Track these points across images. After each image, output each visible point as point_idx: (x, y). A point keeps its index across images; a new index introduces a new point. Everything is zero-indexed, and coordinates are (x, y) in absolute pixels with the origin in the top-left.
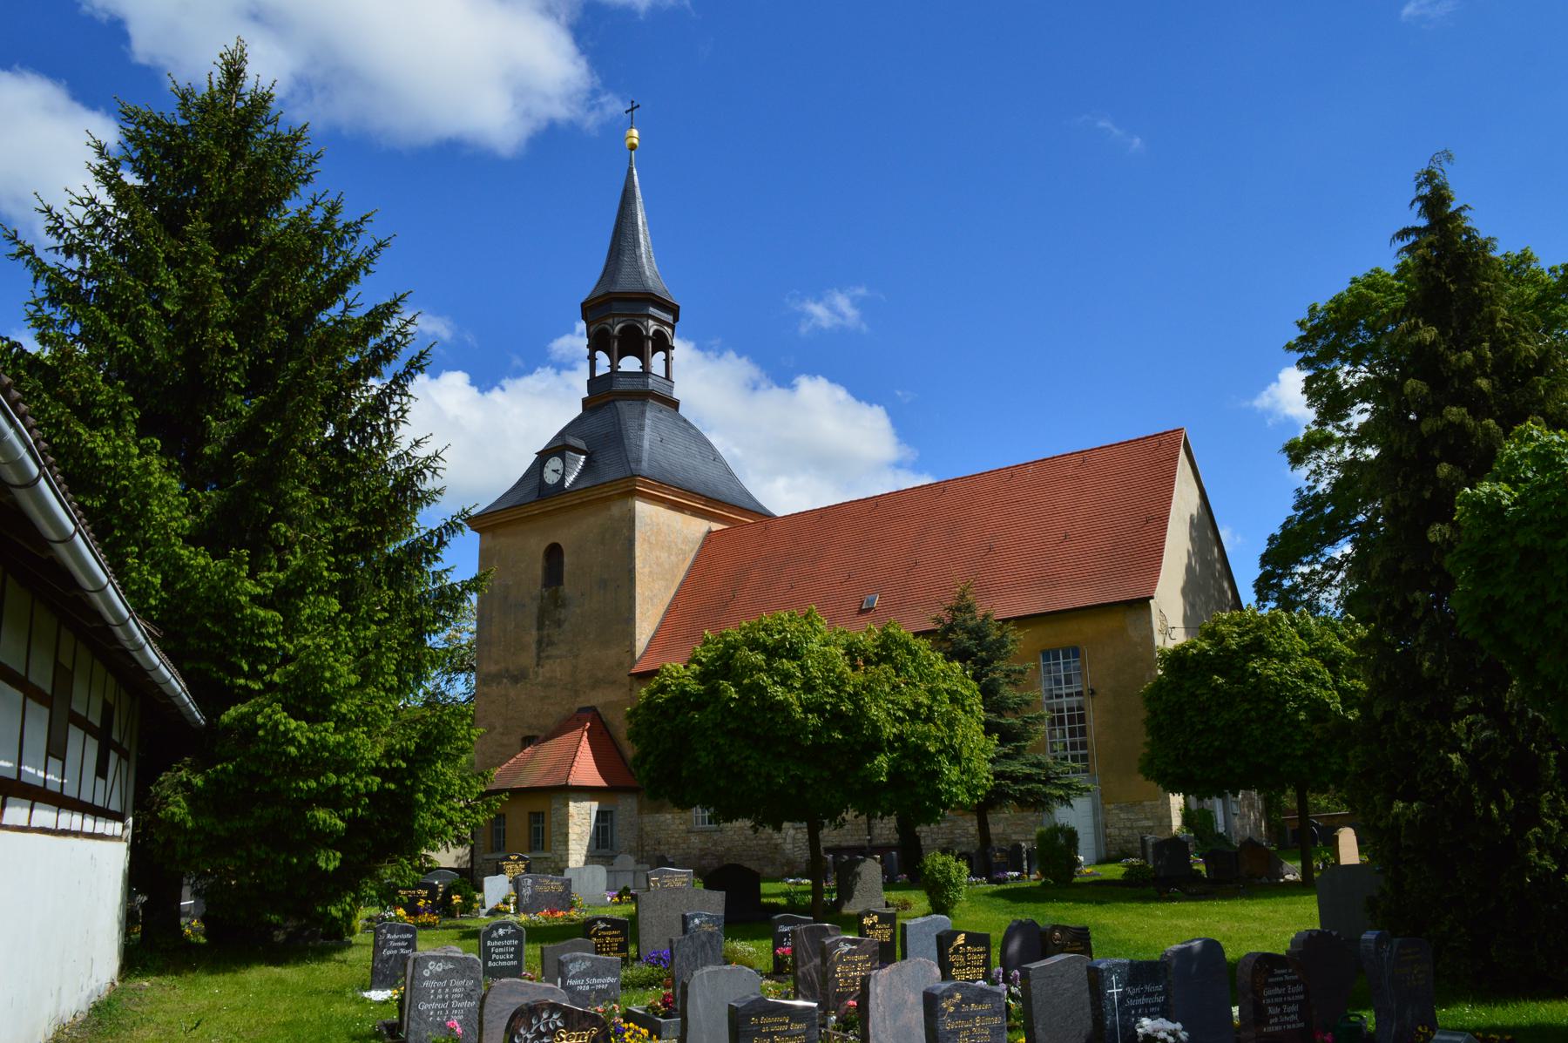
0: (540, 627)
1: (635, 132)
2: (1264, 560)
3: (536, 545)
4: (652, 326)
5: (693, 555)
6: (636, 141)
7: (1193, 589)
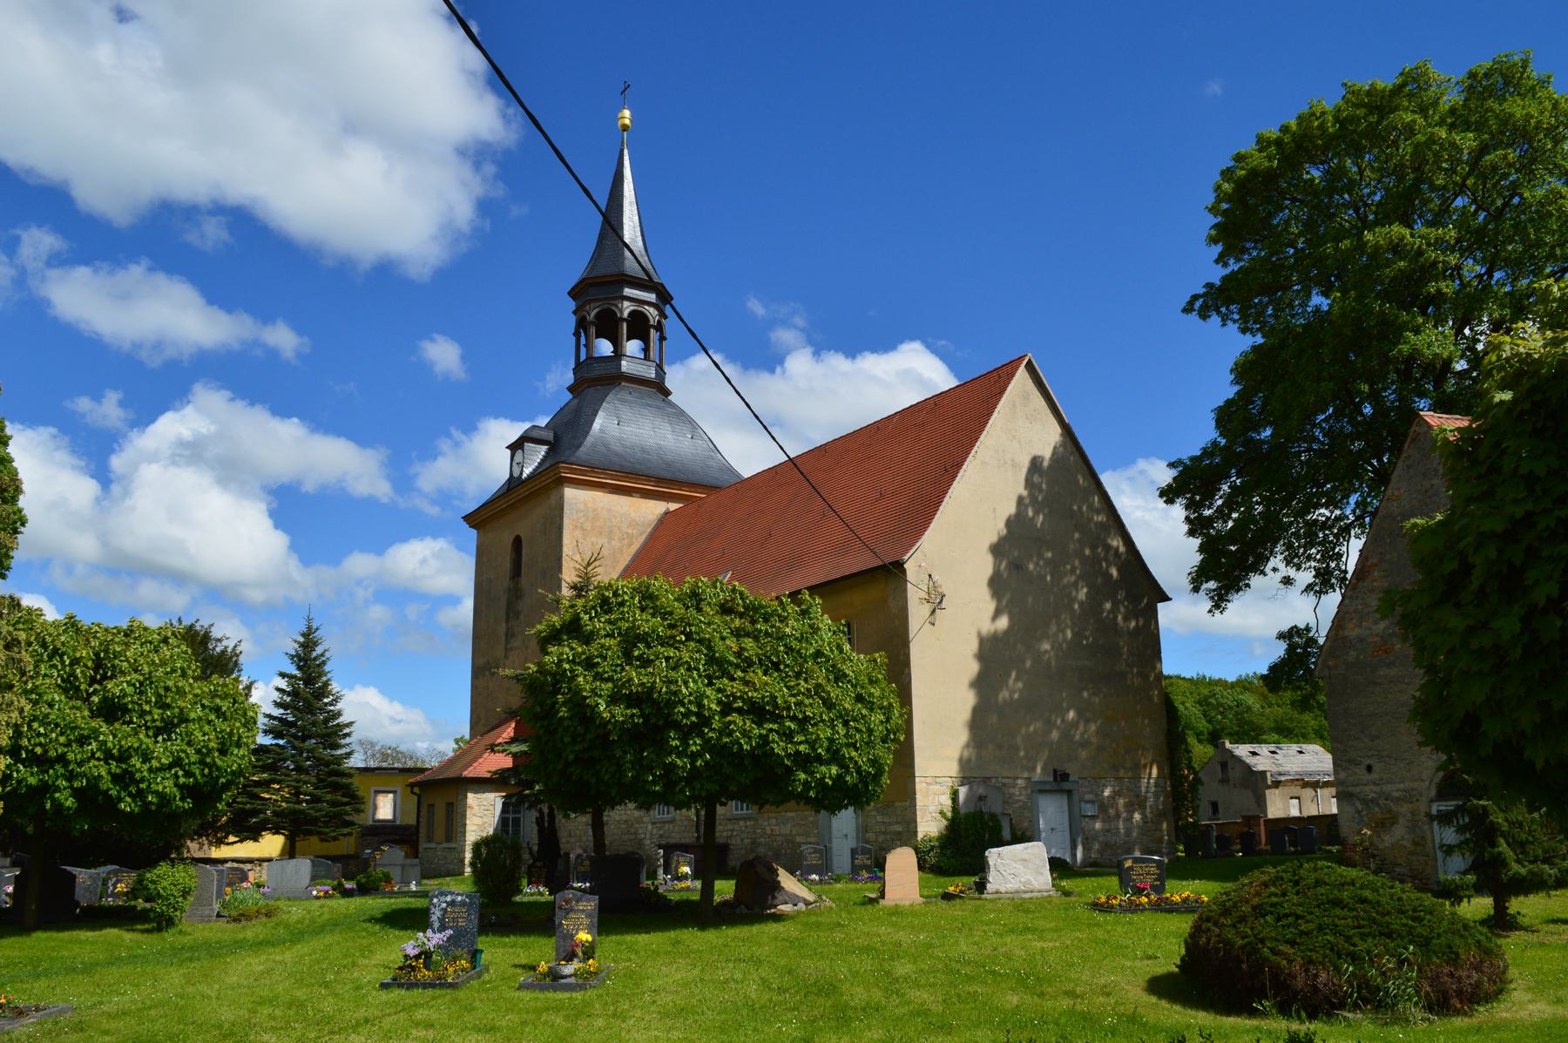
1: (627, 113)
3: (507, 539)
4: (627, 308)
6: (627, 122)
7: (1017, 557)
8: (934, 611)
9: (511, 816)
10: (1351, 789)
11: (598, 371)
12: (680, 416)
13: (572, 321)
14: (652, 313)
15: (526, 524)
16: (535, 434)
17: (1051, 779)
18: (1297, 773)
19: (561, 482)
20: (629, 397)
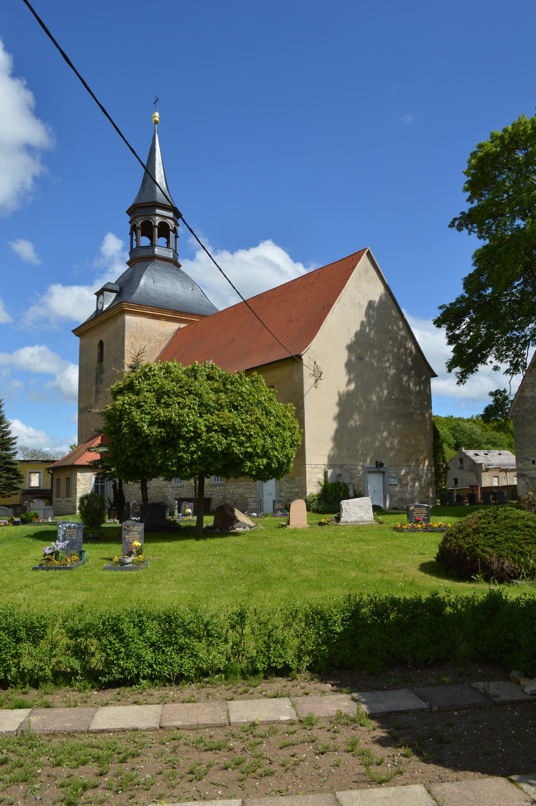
0: (96, 385)
1: (157, 114)
2: (457, 299)
4: (158, 220)
5: (166, 343)
6: (157, 119)
8: (317, 381)
9: (100, 484)
10: (524, 472)
14: (171, 223)
15: (105, 334)
16: (109, 287)
17: (375, 466)
18: (498, 465)
19: (123, 312)
20: (159, 268)
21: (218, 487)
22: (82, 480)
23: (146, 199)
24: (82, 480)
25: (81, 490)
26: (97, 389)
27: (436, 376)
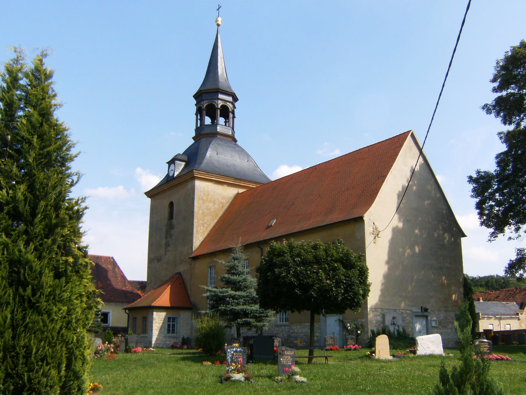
0: (166, 238)
3: (167, 203)
4: (220, 104)
5: (228, 204)
8: (375, 238)
9: (171, 323)
10: (298, 359)
11: (206, 131)
12: (242, 151)
13: (194, 109)
14: (230, 106)
15: (176, 196)
16: (179, 157)
17: (420, 311)
19: (194, 178)
20: (221, 143)
21: (283, 327)
22: (157, 319)
23: (209, 87)
24: (157, 319)
25: (156, 328)
26: (166, 242)
27: (465, 236)
